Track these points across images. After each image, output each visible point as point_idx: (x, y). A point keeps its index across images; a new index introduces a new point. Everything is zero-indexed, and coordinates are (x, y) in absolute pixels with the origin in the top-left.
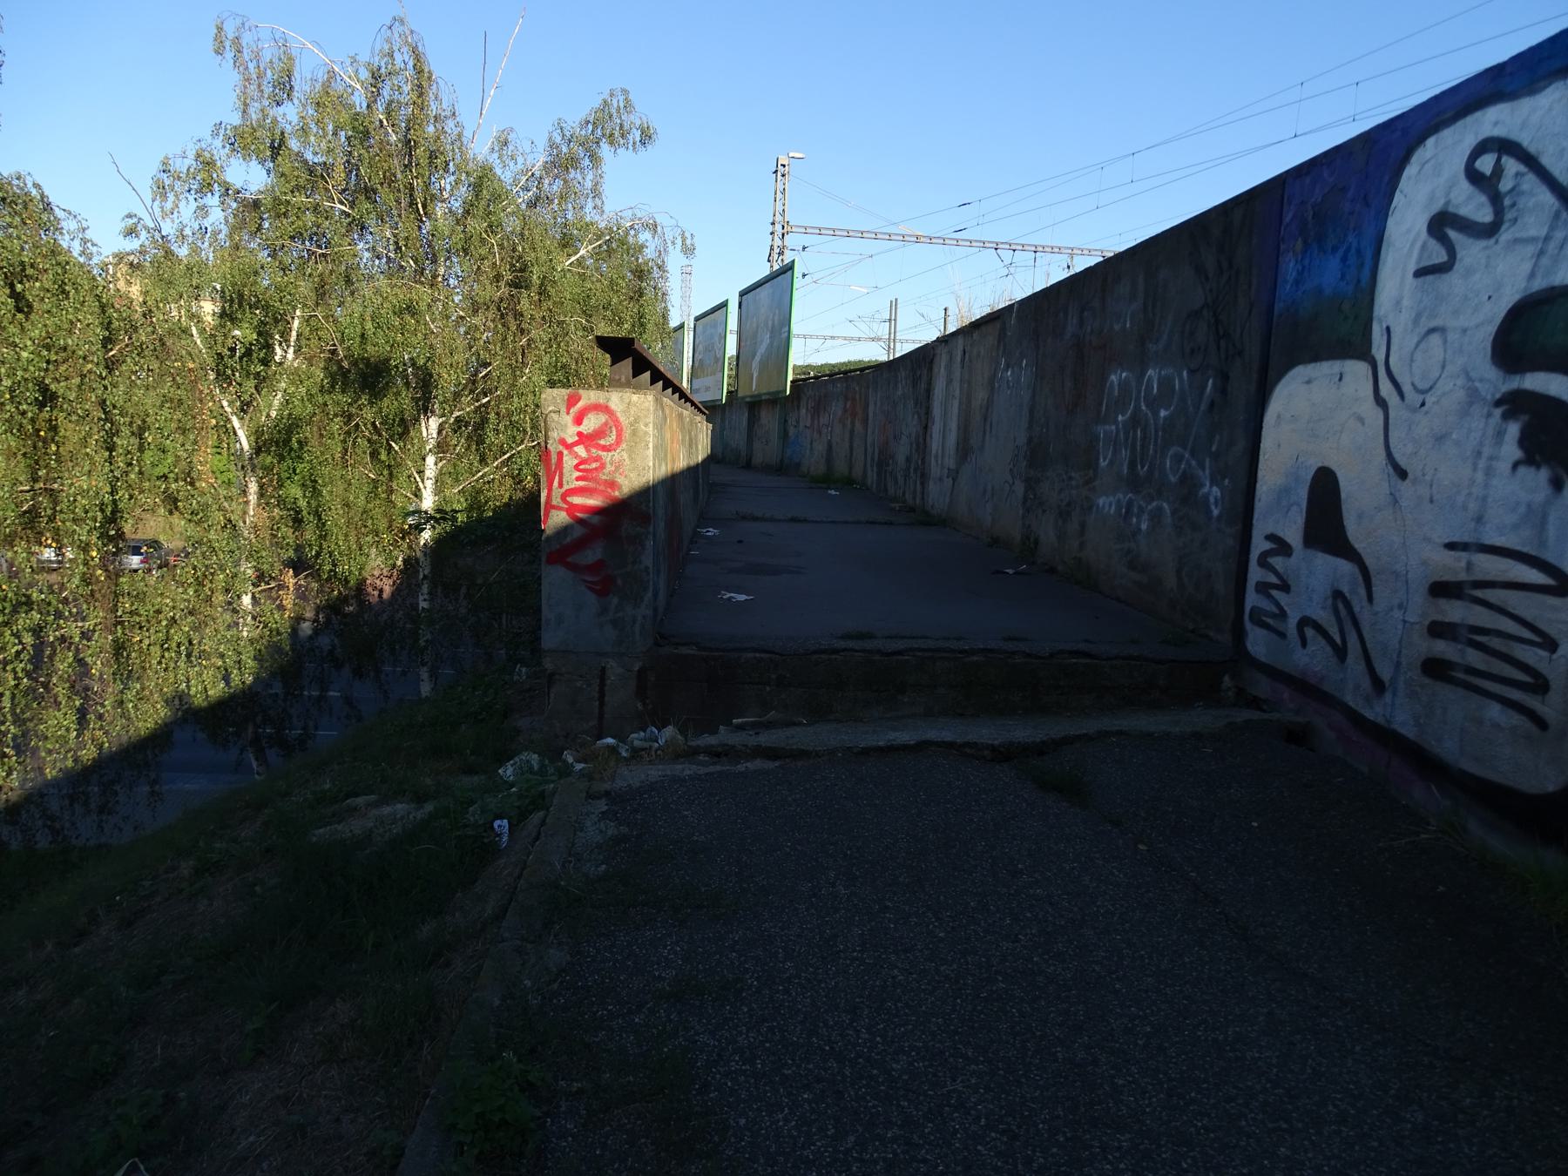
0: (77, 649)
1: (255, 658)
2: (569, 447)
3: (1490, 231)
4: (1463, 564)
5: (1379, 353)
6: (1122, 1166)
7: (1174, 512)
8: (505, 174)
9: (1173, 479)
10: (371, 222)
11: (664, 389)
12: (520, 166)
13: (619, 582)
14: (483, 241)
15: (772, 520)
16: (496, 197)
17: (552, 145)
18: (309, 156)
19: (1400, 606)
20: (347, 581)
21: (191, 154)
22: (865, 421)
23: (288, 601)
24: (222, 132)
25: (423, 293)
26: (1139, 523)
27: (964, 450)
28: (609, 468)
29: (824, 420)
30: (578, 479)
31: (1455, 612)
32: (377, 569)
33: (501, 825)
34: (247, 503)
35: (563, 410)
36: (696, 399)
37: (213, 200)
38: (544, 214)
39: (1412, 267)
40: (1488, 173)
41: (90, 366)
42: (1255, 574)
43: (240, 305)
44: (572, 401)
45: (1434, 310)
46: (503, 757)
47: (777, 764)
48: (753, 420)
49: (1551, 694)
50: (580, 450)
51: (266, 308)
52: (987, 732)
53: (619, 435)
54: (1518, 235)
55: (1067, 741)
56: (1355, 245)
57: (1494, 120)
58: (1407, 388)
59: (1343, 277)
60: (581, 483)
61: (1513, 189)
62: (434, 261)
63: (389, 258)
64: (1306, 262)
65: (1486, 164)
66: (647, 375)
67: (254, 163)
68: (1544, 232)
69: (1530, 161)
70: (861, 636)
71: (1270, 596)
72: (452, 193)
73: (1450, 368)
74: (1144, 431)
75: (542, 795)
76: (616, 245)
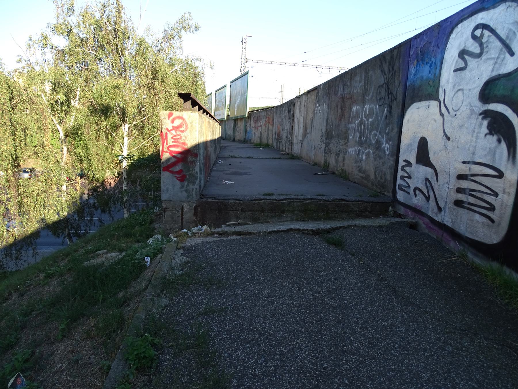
0: (6, 205)
1: (68, 207)
2: (170, 131)
3: (479, 56)
4: (468, 168)
5: (441, 98)
6: (353, 366)
7: (373, 154)
8: (149, 41)
9: (373, 142)
10: (104, 58)
11: (203, 113)
12: (154, 38)
13: (188, 177)
14: (142, 63)
15: (241, 158)
16: (146, 49)
17: (165, 31)
18: (80, 35)
19: (447, 183)
20: (98, 181)
21: (39, 34)
22: (273, 125)
23: (78, 188)
24: (50, 26)
25: (121, 82)
26: (362, 157)
27: (305, 134)
28: (183, 138)
29: (259, 124)
30: (173, 142)
31: (465, 184)
32: (109, 177)
33: (148, 259)
34: (63, 154)
35: (167, 118)
36: (216, 118)
37: (47, 50)
38: (163, 55)
39: (453, 69)
40: (479, 36)
41: (5, 107)
42: (400, 173)
43: (58, 86)
44: (170, 115)
45: (460, 83)
46: (149, 237)
47: (241, 237)
48: (235, 125)
49: (496, 211)
50: (173, 132)
51: (68, 87)
52: (311, 226)
53: (186, 129)
54: (488, 57)
55: (337, 228)
56: (434, 61)
57: (481, 18)
58: (450, 110)
59: (430, 73)
60: (174, 143)
61: (487, 41)
62: (125, 71)
63: (110, 70)
64: (418, 67)
65: (478, 33)
66: (197, 107)
67: (62, 37)
68: (497, 56)
69: (492, 31)
70: (269, 195)
71: (405, 180)
72: (131, 47)
73: (464, 103)
74: (364, 126)
75: (161, 248)
76: (187, 66)
